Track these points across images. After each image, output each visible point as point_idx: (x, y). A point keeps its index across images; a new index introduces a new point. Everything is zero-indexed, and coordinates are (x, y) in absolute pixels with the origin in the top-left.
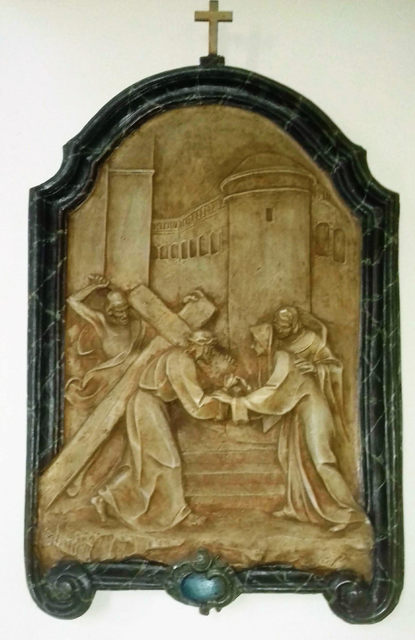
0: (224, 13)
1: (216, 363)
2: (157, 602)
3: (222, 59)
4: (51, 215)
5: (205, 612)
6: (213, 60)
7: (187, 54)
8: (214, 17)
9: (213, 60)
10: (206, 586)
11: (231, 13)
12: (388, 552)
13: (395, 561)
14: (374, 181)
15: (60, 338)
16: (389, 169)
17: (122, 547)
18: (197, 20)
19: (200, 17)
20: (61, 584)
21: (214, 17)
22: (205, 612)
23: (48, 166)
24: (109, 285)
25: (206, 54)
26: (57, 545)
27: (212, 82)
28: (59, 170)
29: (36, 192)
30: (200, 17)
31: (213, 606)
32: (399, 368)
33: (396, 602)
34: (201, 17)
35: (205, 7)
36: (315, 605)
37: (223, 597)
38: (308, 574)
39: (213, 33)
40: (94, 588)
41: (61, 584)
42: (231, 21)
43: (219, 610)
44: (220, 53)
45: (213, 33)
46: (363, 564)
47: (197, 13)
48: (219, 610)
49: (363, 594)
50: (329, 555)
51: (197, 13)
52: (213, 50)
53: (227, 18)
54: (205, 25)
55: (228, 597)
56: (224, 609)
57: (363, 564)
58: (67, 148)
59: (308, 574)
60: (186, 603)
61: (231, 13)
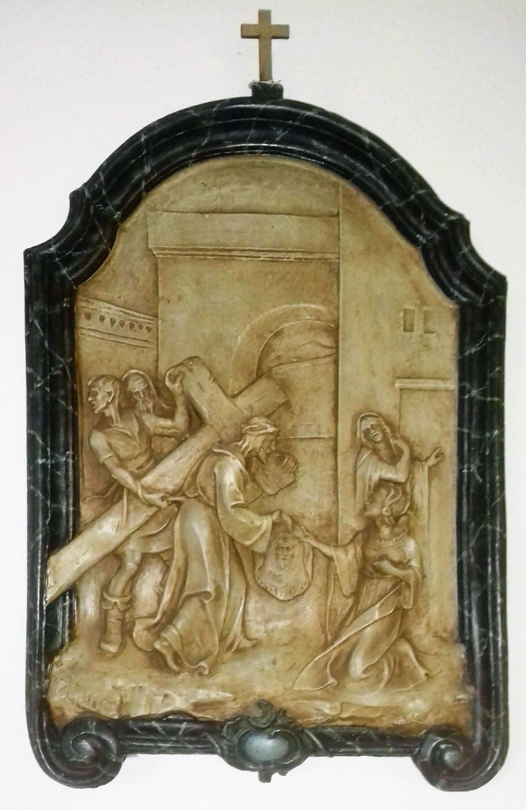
0: (279, 27)
2: (208, 768)
3: (278, 90)
4: (56, 279)
5: (265, 778)
6: (266, 91)
7: (230, 80)
8: (265, 32)
9: (266, 91)
10: (265, 745)
11: (287, 28)
14: (472, 251)
16: (495, 244)
18: (243, 37)
19: (247, 33)
20: (75, 745)
21: (265, 32)
22: (265, 778)
23: (49, 220)
27: (262, 125)
29: (27, 252)
30: (247, 33)
32: (58, 549)
33: (498, 769)
40: (124, 751)
42: (287, 38)
47: (243, 27)
49: (460, 752)
50: (417, 706)
51: (243, 27)
53: (283, 33)
54: (255, 43)
55: (296, 757)
56: (292, 773)
61: (287, 28)
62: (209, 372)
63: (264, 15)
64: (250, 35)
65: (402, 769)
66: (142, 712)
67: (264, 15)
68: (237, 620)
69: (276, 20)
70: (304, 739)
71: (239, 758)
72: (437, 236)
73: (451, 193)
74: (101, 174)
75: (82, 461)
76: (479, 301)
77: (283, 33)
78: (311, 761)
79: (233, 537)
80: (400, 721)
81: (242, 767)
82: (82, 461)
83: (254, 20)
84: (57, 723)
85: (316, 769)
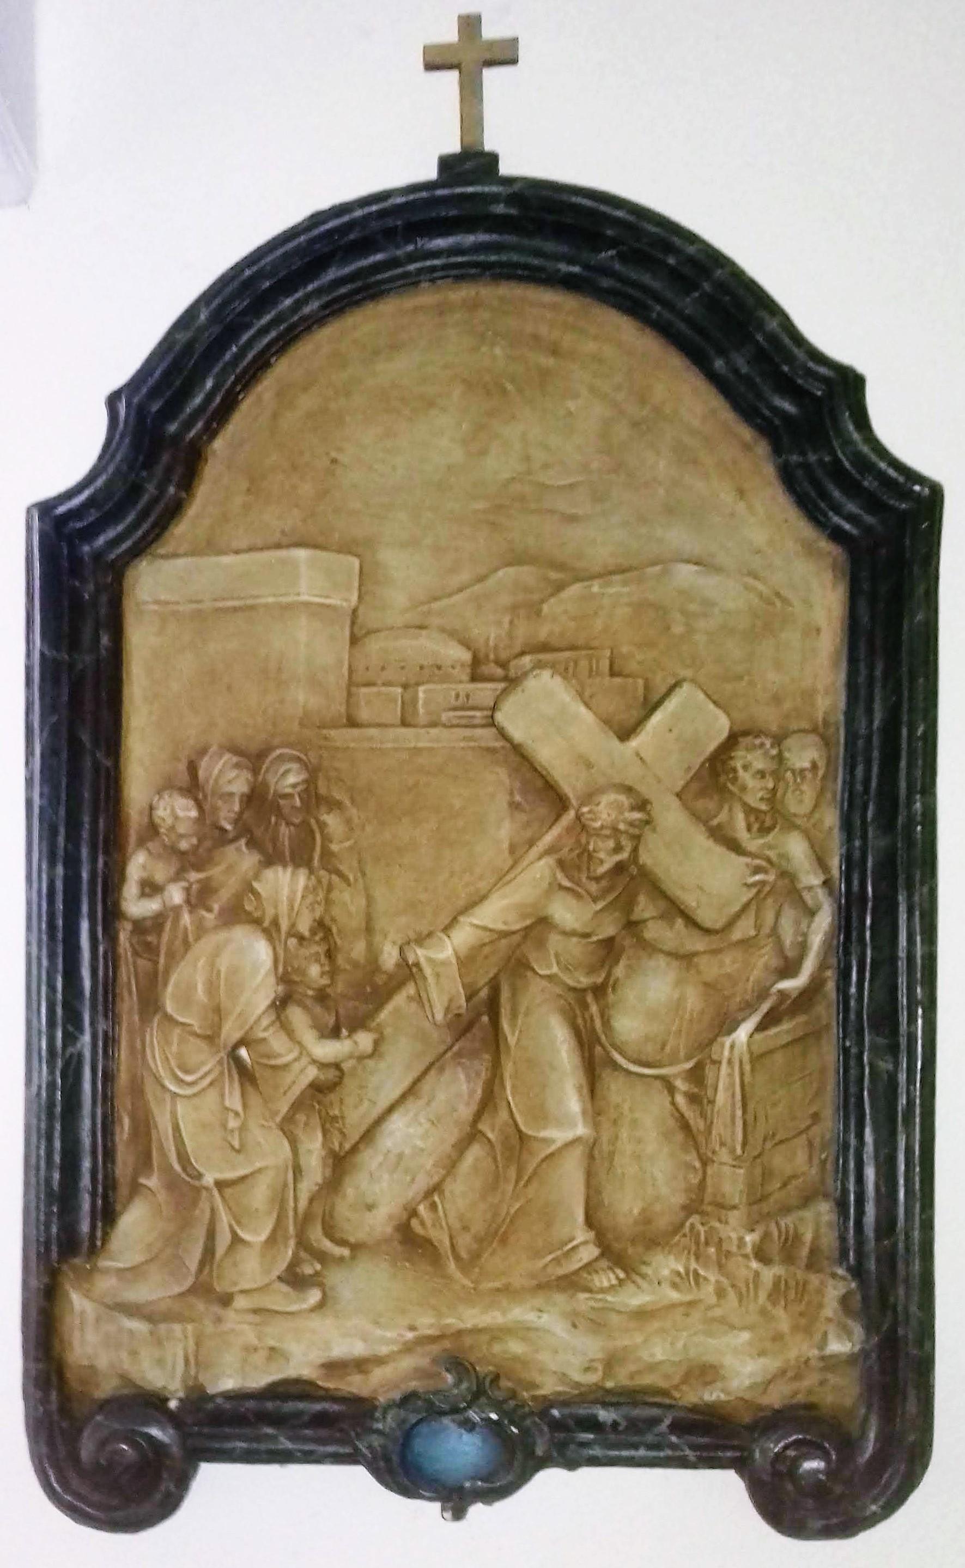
2: (343, 1492)
3: (493, 159)
4: (84, 562)
6: (470, 165)
7: (405, 155)
9: (470, 165)
11: (514, 42)
13: (843, 901)
15: (243, 270)
16: (910, 424)
17: (259, 1358)
18: (431, 66)
19: (436, 61)
20: (117, 1456)
21: (471, 56)
22: (459, 1514)
23: (69, 449)
24: (169, 1018)
25: (453, 146)
27: (490, 231)
29: (45, 509)
34: (438, 60)
37: (499, 1481)
38: (617, 266)
39: (471, 94)
41: (117, 1456)
42: (514, 61)
45: (471, 94)
46: (842, 1393)
50: (743, 1368)
52: (468, 139)
53: (504, 54)
57: (842, 1393)
58: (112, 401)
59: (617, 266)
61: (514, 42)
62: (545, 309)
63: (470, 25)
65: (721, 1493)
66: (229, 1384)
67: (470, 25)
69: (489, 32)
70: (542, 1433)
71: (403, 1472)
72: (798, 408)
73: (827, 322)
74: (108, 763)
76: (882, 532)
77: (504, 54)
78: (549, 1480)
79: (627, 783)
80: (712, 1395)
81: (407, 1491)
83: (450, 35)
84: (608, 1071)
85: (552, 1490)
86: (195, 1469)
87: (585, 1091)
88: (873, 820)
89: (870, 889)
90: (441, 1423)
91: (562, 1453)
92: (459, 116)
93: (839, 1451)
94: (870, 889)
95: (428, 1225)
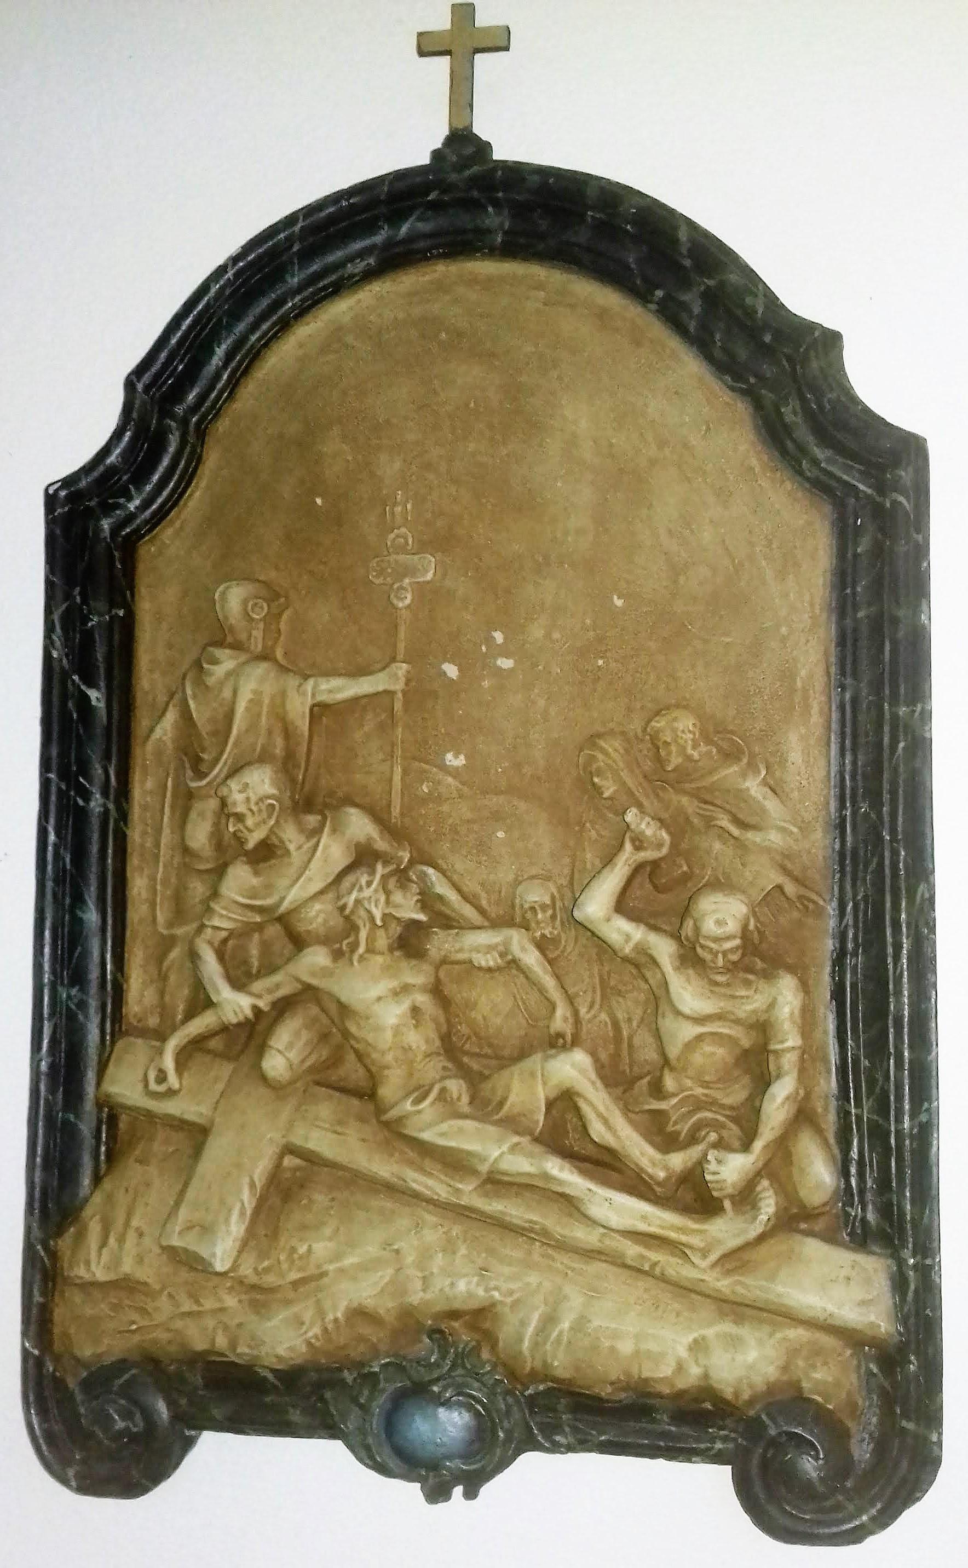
1: (306, 1110)
2: (317, 1466)
3: (485, 148)
4: (93, 538)
5: (438, 1493)
6: (463, 145)
7: (408, 140)
8: (462, 44)
9: (463, 145)
12: (906, 1368)
16: (880, 381)
18: (422, 53)
19: (427, 47)
21: (462, 44)
22: (438, 1493)
23: (83, 424)
26: (99, 1336)
27: (467, 207)
28: (89, 463)
31: (456, 1480)
33: (937, 1280)
35: (441, 21)
36: (703, 1489)
39: (462, 92)
41: (112, 1421)
42: (507, 49)
43: (471, 1494)
44: (481, 129)
48: (471, 1494)
53: (499, 42)
54: (442, 64)
56: (487, 1490)
60: (361, 1460)
63: (463, 14)
64: (437, 49)
67: (463, 14)
68: (831, 1047)
69: (441, 21)
71: (391, 1453)
73: (801, 289)
75: (829, 772)
78: (531, 1464)
82: (829, 772)
85: (536, 1475)
86: (189, 1443)
87: (630, 1229)
88: (872, 872)
89: (893, 1164)
90: (436, 1417)
91: (548, 1438)
92: (449, 71)
93: (831, 1449)
94: (893, 1164)
95: (283, 946)
